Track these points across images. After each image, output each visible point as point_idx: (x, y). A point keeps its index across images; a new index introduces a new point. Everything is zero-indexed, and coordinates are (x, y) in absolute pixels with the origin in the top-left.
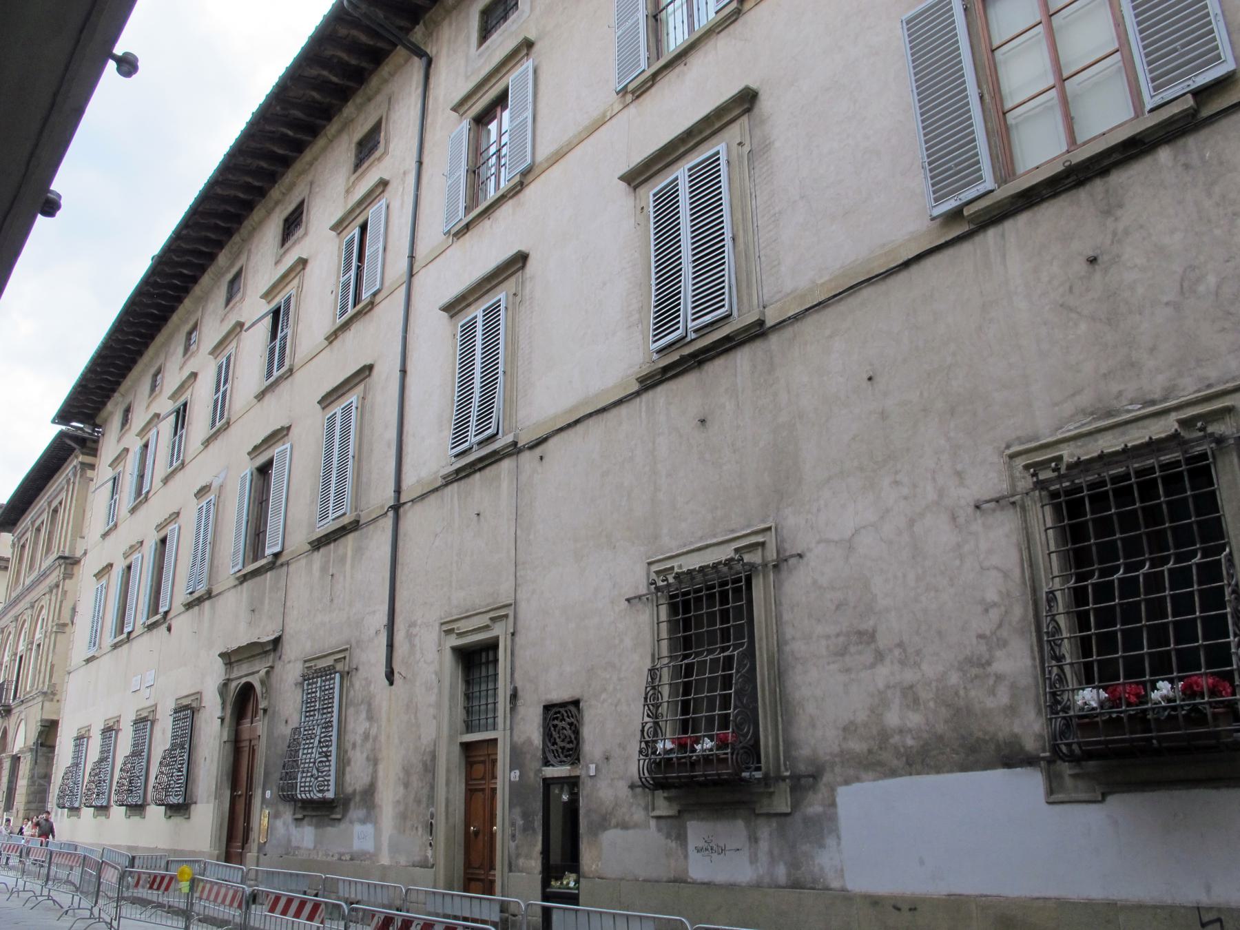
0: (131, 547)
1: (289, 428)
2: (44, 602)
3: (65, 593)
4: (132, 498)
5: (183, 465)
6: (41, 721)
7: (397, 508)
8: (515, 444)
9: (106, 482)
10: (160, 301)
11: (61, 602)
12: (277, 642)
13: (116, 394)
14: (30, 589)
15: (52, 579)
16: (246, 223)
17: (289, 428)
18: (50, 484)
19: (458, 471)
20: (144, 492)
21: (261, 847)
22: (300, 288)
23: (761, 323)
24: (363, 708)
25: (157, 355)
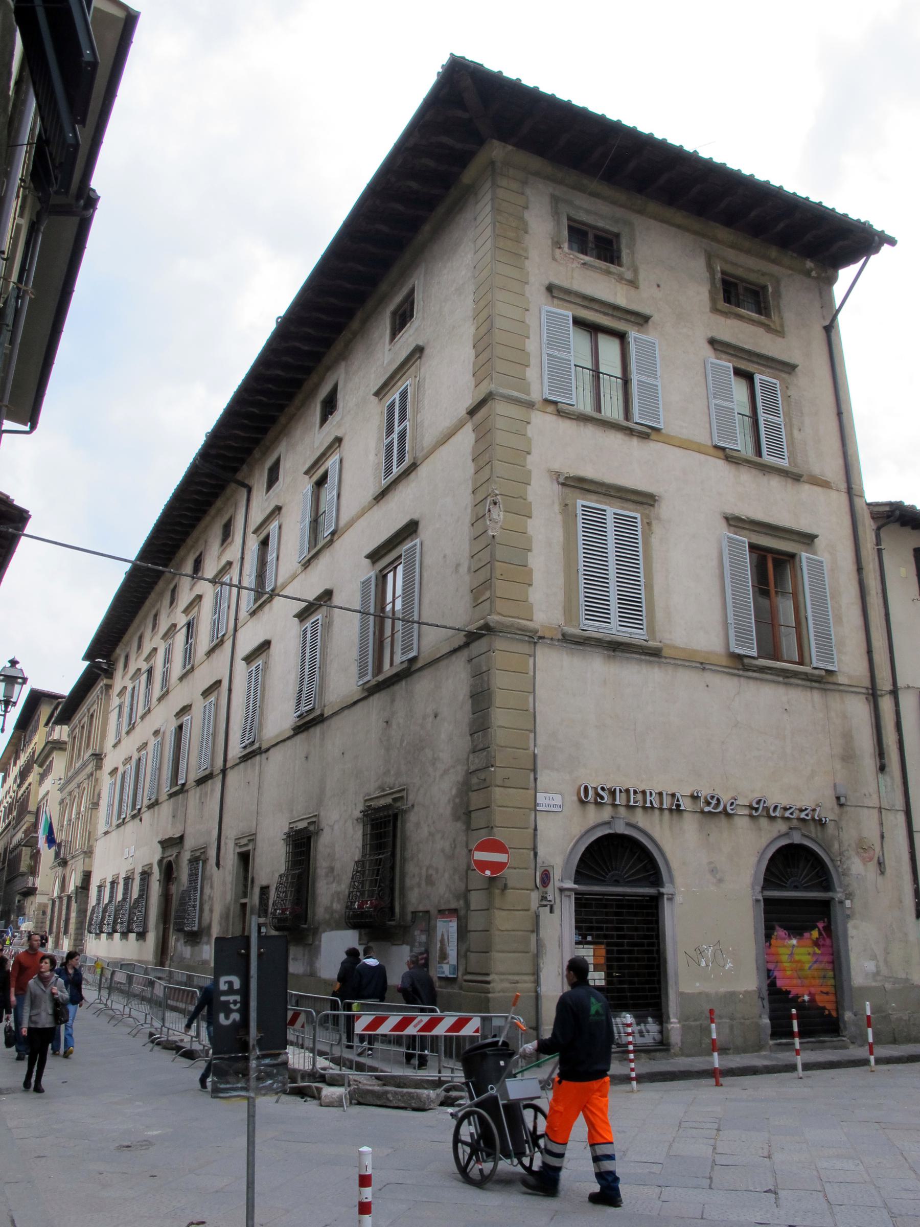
0: (126, 759)
1: (191, 705)
2: (85, 785)
3: (97, 780)
4: (252, 601)
5: (192, 669)
6: (84, 871)
7: (224, 771)
8: (260, 748)
9: (182, 628)
10: (237, 432)
11: (95, 786)
12: (181, 838)
13: (121, 644)
14: (77, 773)
15: (90, 768)
16: (177, 555)
17: (191, 705)
18: (89, 695)
19: (244, 756)
20: (220, 635)
21: (172, 957)
22: (199, 612)
23: (322, 715)
24: (209, 881)
25: (139, 627)
